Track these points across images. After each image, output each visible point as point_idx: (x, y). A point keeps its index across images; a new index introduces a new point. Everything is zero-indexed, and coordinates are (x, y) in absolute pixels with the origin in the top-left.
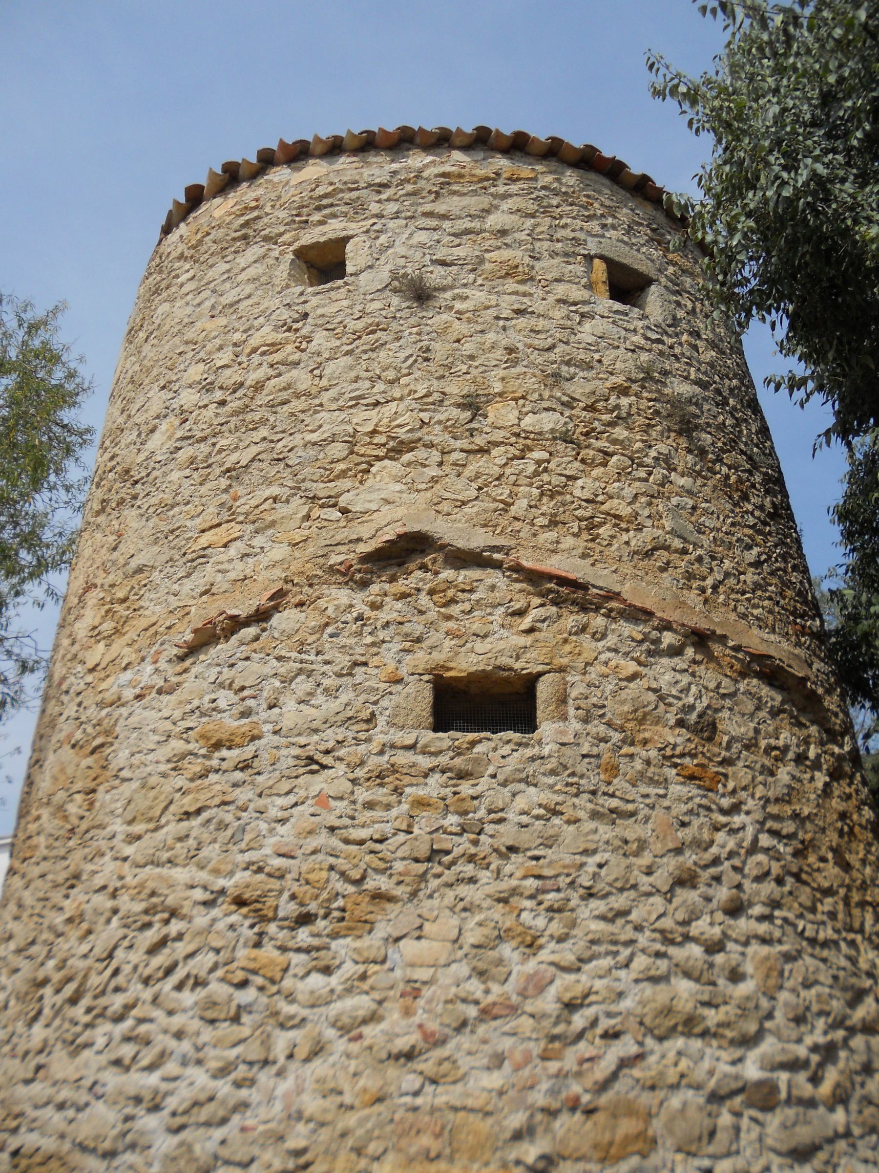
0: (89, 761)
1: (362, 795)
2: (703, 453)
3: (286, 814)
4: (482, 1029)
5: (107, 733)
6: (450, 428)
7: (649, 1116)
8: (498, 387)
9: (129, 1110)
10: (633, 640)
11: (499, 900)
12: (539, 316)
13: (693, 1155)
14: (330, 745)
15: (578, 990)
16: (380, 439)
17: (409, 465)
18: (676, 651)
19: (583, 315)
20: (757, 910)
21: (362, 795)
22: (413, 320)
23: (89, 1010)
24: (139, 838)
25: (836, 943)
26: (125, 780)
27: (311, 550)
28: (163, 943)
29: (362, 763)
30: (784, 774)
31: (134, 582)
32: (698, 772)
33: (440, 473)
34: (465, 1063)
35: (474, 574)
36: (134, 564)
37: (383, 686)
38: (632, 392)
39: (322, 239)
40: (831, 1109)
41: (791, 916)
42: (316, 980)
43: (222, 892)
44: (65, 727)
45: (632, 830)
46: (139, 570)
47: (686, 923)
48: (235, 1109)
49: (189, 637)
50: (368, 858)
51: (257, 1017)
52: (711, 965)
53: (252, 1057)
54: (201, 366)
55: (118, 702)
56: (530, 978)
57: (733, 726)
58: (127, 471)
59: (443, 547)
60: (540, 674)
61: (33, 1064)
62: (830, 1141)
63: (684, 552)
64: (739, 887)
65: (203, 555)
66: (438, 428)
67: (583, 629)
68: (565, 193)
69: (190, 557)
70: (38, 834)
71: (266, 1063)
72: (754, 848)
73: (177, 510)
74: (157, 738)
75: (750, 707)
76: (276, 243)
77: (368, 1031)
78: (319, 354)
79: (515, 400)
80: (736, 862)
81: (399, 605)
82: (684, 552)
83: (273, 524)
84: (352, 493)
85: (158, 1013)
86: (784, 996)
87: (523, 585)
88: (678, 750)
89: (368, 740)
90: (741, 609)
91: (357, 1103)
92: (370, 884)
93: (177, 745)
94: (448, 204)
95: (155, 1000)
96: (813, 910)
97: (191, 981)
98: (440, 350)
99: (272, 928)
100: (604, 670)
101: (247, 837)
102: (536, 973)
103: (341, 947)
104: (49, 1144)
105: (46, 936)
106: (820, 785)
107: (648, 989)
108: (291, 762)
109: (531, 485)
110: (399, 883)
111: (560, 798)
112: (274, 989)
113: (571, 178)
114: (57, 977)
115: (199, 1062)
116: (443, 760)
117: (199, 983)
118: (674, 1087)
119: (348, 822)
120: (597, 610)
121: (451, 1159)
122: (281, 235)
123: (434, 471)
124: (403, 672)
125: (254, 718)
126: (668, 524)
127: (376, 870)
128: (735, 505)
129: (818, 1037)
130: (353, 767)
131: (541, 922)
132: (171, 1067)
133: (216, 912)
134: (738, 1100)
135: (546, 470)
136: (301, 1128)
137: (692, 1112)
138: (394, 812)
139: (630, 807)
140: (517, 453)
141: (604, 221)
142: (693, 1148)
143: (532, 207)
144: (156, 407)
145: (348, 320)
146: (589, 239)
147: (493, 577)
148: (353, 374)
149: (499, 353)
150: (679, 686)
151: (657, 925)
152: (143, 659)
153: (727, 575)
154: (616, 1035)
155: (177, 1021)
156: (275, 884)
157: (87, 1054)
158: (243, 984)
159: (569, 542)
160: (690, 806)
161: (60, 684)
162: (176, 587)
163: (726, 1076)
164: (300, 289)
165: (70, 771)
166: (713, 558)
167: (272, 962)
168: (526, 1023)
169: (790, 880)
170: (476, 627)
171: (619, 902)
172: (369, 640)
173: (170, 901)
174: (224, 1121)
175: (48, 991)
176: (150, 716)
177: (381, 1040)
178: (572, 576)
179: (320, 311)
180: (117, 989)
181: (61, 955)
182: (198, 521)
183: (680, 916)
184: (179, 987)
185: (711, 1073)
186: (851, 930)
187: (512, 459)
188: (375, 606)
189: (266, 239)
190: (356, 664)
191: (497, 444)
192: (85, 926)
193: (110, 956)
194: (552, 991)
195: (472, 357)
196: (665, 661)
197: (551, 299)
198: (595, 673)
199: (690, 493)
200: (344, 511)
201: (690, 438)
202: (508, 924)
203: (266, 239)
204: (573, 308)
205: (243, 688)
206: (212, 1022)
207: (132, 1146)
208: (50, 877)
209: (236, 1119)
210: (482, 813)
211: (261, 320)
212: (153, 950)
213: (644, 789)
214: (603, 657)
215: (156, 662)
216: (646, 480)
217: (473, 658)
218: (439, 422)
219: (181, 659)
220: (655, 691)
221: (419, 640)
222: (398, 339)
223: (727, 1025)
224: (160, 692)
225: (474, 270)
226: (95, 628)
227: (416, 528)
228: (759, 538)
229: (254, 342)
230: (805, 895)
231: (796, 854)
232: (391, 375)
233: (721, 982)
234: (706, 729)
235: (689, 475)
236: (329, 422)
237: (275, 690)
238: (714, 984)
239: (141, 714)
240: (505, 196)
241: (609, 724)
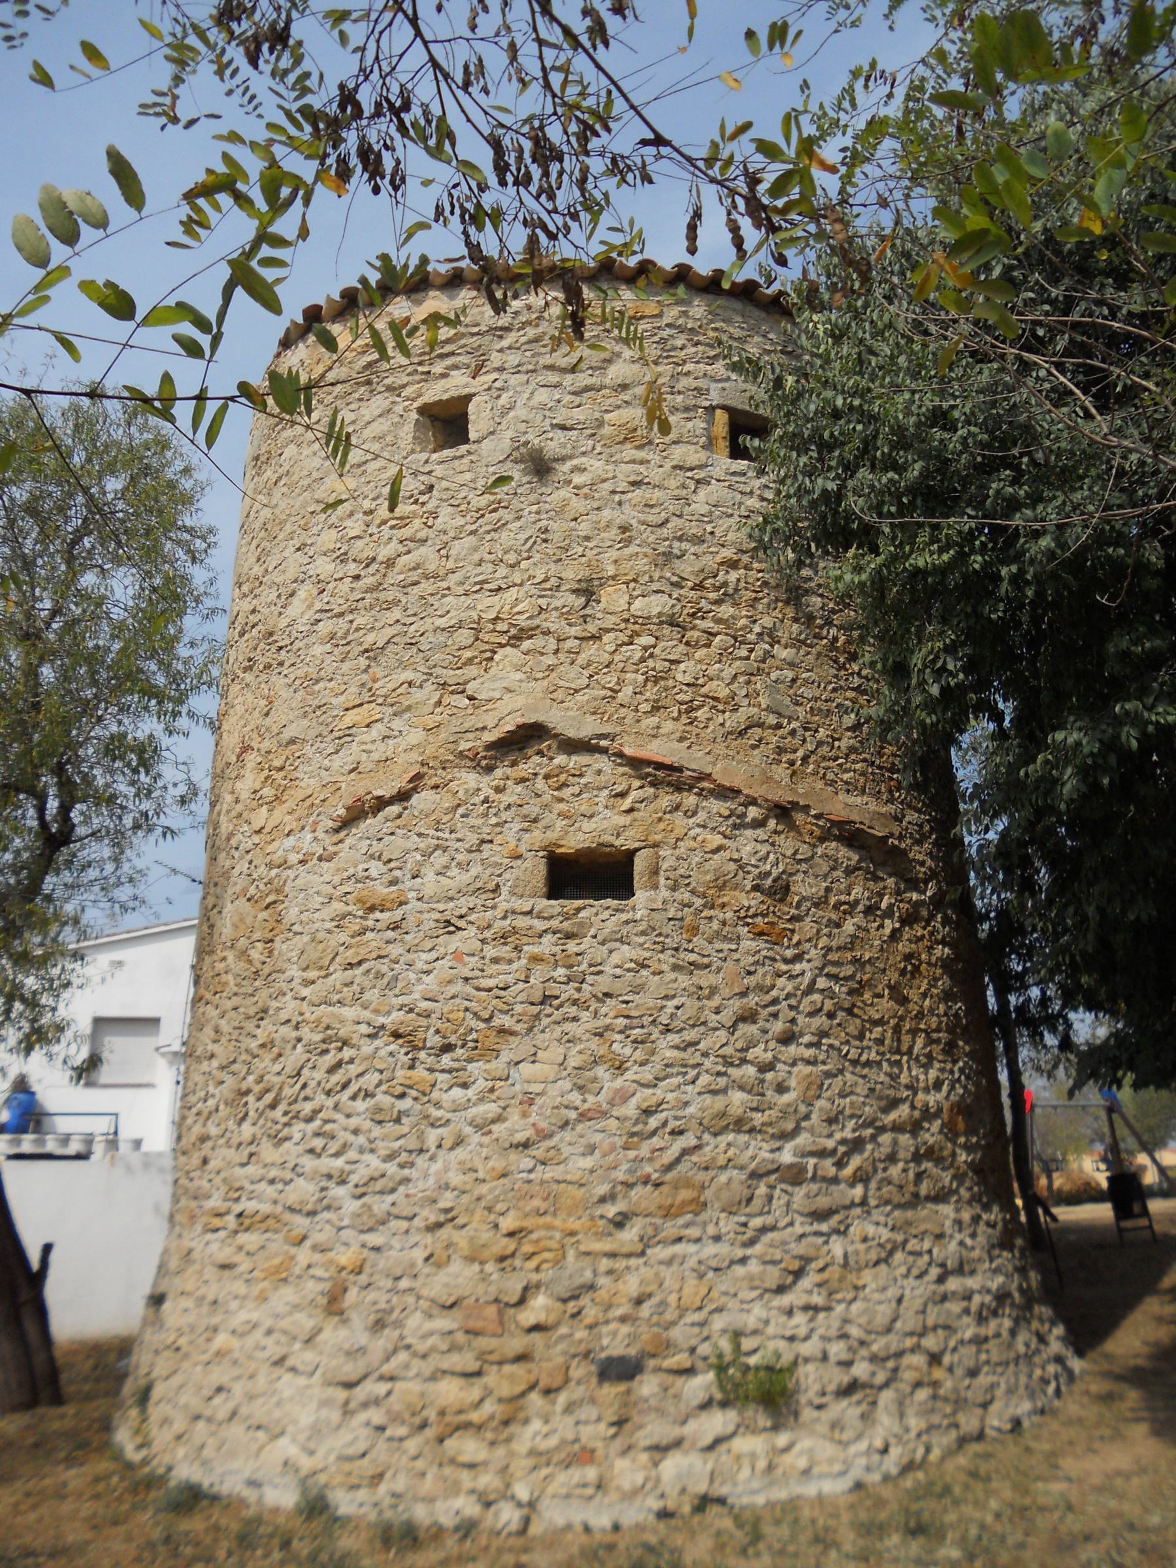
1: (490, 952)
2: (810, 618)
4: (580, 1128)
5: (278, 891)
6: (565, 615)
7: (703, 1188)
8: (611, 570)
9: (323, 1184)
14: (463, 911)
15: (653, 1101)
18: (759, 824)
19: (698, 482)
20: (806, 1039)
21: (490, 952)
22: (533, 497)
23: (286, 1113)
25: (879, 1064)
27: (443, 735)
28: (339, 1064)
29: (489, 926)
30: (849, 927)
31: (288, 752)
32: (766, 928)
34: (566, 1151)
36: (287, 735)
39: (445, 397)
40: (852, 1185)
41: (837, 1043)
42: (457, 1092)
43: (383, 1027)
45: (705, 979)
46: (292, 741)
47: (746, 1050)
48: (400, 1183)
49: (342, 812)
51: (413, 1119)
52: (762, 1081)
54: (334, 532)
55: (284, 864)
56: (617, 1091)
57: (804, 887)
59: (556, 736)
61: (246, 1153)
62: (847, 1207)
63: (779, 726)
64: (793, 1021)
65: (349, 733)
67: (677, 808)
72: (811, 989)
73: (321, 685)
75: (825, 868)
77: (495, 1128)
79: (627, 583)
80: (793, 1002)
81: (519, 789)
82: (779, 726)
83: (409, 708)
85: (338, 1116)
86: (821, 1103)
89: (494, 907)
90: (830, 776)
92: (496, 1022)
93: (338, 907)
95: (336, 1107)
96: (861, 1037)
98: (558, 528)
99: (422, 1055)
100: (693, 844)
101: (400, 985)
103: (475, 1068)
104: (265, 1208)
105: (244, 1057)
106: (887, 931)
107: (708, 1099)
108: (433, 924)
111: (647, 954)
113: (699, 308)
114: (257, 1089)
115: (372, 1151)
116: (554, 923)
117: (368, 1095)
118: (724, 1168)
121: (555, 1214)
122: (404, 386)
123: (549, 660)
124: (522, 849)
125: (400, 886)
126: (764, 701)
128: (842, 667)
129: (848, 1134)
130: (482, 929)
131: (627, 1051)
132: (352, 1154)
133: (378, 1043)
134: (773, 1177)
135: (651, 655)
136: (449, 1195)
137: (735, 1185)
138: (515, 966)
144: (292, 572)
146: (713, 385)
147: (602, 762)
148: (477, 557)
153: (820, 744)
154: (681, 1132)
155: (353, 1122)
156: (423, 1022)
157: (287, 1145)
158: (402, 1096)
159: (669, 726)
161: (228, 839)
162: (326, 762)
164: (424, 456)
165: (249, 920)
167: (423, 1080)
168: (612, 1124)
169: (841, 1015)
171: (690, 1035)
172: (494, 820)
173: (342, 1033)
174: (393, 1190)
175: (251, 1099)
177: (504, 1135)
178: (667, 761)
180: (306, 1099)
181: (258, 1072)
182: (342, 698)
183: (739, 1045)
184: (354, 1098)
185: (753, 1158)
186: (898, 1051)
188: (499, 790)
189: (390, 389)
190: (483, 841)
192: (276, 1050)
193: (299, 1074)
194: (634, 1101)
195: (587, 538)
196: (749, 833)
197: (668, 465)
198: (687, 845)
199: (792, 665)
200: (471, 698)
201: (798, 606)
203: (390, 389)
207: (328, 1208)
209: (402, 1189)
212: (331, 1070)
213: (718, 945)
214: (692, 833)
221: (535, 821)
222: (519, 518)
223: (770, 1124)
224: (320, 859)
227: (531, 719)
230: (853, 1026)
231: (851, 992)
232: (511, 558)
233: (769, 1093)
234: (780, 891)
235: (793, 646)
236: (455, 607)
237: (418, 863)
239: (304, 877)
241: (693, 892)
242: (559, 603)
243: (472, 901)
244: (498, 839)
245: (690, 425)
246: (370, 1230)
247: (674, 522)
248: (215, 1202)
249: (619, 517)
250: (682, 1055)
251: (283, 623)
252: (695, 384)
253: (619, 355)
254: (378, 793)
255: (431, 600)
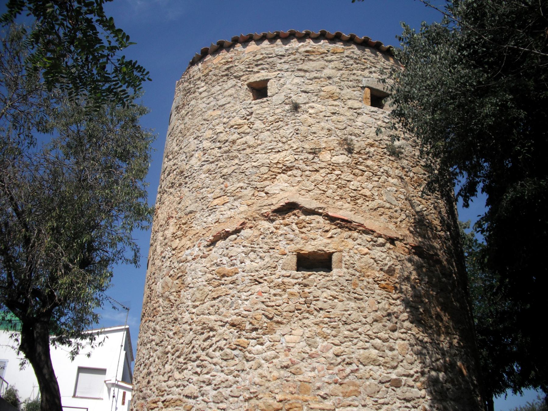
0: (177, 281)
1: (273, 291)
3: (248, 298)
5: (182, 272)
8: (324, 145)
10: (367, 241)
11: (316, 324)
12: (341, 115)
13: (372, 397)
14: (262, 275)
15: (340, 351)
16: (280, 166)
17: (290, 176)
18: (383, 245)
19: (358, 114)
21: (273, 291)
23: (185, 359)
24: (197, 306)
26: (190, 288)
27: (255, 207)
28: (208, 338)
29: (272, 282)
32: (386, 286)
33: (301, 179)
34: (304, 369)
35: (312, 217)
36: (188, 210)
37: (280, 256)
38: (375, 145)
39: (258, 80)
41: (414, 333)
42: (259, 347)
43: (227, 322)
44: (165, 269)
46: (191, 212)
48: (234, 383)
49: (212, 238)
50: (275, 311)
53: (239, 369)
54: (211, 131)
55: (186, 261)
58: (182, 172)
60: (333, 253)
63: (390, 208)
66: (301, 161)
68: (356, 59)
69: (210, 208)
70: (159, 307)
71: (243, 370)
73: (204, 190)
74: (201, 273)
76: (239, 80)
78: (257, 130)
79: (330, 150)
81: (285, 228)
82: (390, 208)
84: (270, 186)
87: (328, 221)
88: (379, 279)
91: (271, 380)
94: (306, 66)
97: (218, 349)
98: (303, 129)
101: (234, 305)
102: (327, 346)
104: (175, 397)
107: (362, 351)
109: (334, 184)
110: (284, 319)
111: (337, 294)
112: (245, 350)
116: (300, 281)
119: (268, 300)
120: (355, 230)
123: (299, 179)
125: (236, 267)
127: (277, 315)
128: (415, 189)
133: (225, 328)
135: (339, 178)
139: (361, 297)
140: (329, 172)
141: (371, 70)
142: (372, 395)
143: (341, 65)
144: (193, 147)
145: (268, 116)
146: (364, 79)
148: (270, 139)
149: (325, 132)
150: (382, 257)
151: (367, 333)
152: (194, 246)
154: (351, 364)
155: (215, 360)
157: (185, 371)
159: (347, 205)
160: (382, 297)
163: (385, 376)
166: (402, 210)
170: (311, 236)
171: (354, 326)
172: (275, 240)
173: (210, 325)
174: (231, 386)
175: (169, 355)
176: (200, 266)
178: (346, 218)
179: (257, 112)
182: (212, 195)
185: (380, 375)
187: (327, 174)
190: (271, 248)
191: (322, 168)
193: (191, 343)
194: (331, 351)
195: (315, 133)
196: (378, 248)
200: (267, 193)
202: (318, 331)
204: (355, 111)
205: (232, 256)
206: (226, 360)
208: (166, 320)
210: (311, 298)
211: (235, 114)
212: (205, 340)
213: (366, 291)
214: (356, 247)
215: (199, 247)
216: (378, 181)
217: (310, 247)
218: (302, 159)
219: (208, 246)
220: (373, 259)
222: (287, 125)
224: (201, 258)
225: (317, 95)
226: (174, 233)
227: (291, 200)
228: (424, 201)
229: (232, 123)
236: (262, 158)
238: (384, 351)
240: (330, 61)
242: (302, 157)
243: (266, 272)
244: (277, 247)
245: (355, 93)
246: (222, 402)
247: (349, 128)
248: (154, 398)
249: (327, 126)
250: (351, 333)
251: (188, 167)
252: (357, 78)
253: (327, 66)
254: (227, 230)
255: (251, 155)
